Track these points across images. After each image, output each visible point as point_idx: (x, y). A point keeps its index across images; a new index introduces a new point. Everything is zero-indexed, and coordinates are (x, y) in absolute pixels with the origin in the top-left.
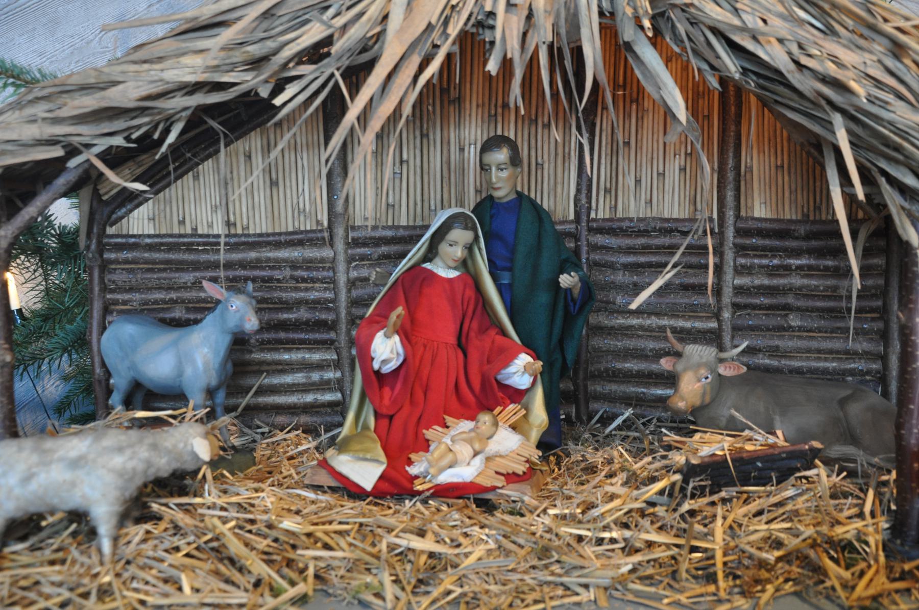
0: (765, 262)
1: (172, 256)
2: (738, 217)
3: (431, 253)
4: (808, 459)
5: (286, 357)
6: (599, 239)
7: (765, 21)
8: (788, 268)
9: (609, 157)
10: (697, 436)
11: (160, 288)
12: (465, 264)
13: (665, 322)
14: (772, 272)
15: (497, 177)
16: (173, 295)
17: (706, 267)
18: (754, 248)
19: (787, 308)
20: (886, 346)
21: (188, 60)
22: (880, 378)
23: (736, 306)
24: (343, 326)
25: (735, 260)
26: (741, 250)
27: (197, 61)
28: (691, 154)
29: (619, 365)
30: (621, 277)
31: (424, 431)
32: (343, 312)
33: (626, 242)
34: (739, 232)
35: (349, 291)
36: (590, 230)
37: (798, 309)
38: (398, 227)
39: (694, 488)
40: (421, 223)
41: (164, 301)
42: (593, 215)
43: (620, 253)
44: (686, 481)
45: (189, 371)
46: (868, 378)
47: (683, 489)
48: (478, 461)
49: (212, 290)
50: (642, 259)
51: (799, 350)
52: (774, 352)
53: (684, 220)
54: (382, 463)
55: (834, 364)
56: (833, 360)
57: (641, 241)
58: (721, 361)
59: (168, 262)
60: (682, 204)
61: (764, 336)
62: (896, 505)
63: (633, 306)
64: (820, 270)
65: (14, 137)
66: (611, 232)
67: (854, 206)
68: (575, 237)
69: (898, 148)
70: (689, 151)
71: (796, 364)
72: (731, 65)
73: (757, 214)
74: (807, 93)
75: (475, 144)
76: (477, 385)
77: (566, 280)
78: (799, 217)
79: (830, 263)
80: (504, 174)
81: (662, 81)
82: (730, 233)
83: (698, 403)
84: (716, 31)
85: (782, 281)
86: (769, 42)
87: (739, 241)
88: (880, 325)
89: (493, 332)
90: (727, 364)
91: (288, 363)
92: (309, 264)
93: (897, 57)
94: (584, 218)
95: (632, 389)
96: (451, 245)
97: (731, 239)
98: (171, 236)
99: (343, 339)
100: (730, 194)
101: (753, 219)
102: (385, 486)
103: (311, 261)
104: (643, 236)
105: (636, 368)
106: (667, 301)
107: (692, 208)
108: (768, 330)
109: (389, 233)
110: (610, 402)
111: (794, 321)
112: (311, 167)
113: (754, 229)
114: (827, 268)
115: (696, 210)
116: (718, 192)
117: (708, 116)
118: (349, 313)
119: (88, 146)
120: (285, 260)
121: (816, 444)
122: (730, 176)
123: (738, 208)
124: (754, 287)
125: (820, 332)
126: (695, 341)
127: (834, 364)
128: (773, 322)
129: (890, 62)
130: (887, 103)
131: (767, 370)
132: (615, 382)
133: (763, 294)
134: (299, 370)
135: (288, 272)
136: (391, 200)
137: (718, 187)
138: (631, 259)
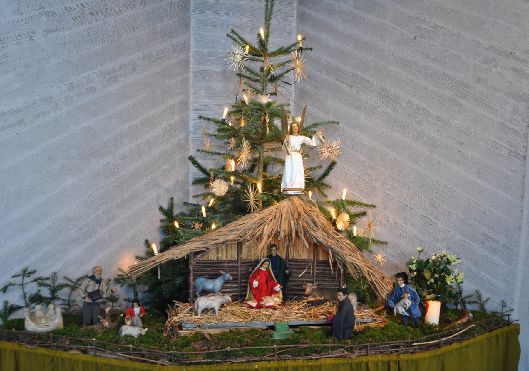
0: (322, 268)
1: (206, 265)
2: (317, 259)
3: (261, 266)
5: (228, 285)
6: (290, 263)
8: (326, 269)
10: (309, 298)
11: (203, 271)
12: (267, 269)
13: (303, 279)
14: (323, 270)
16: (206, 273)
17: (311, 269)
18: (320, 265)
19: (325, 277)
21: (231, 236)
23: (316, 276)
24: (239, 279)
26: (317, 266)
27: (232, 236)
29: (294, 288)
30: (295, 270)
32: (240, 277)
34: (317, 262)
35: (241, 272)
36: (289, 261)
37: (327, 277)
41: (204, 274)
42: (289, 258)
44: (307, 304)
45: (216, 288)
47: (307, 306)
49: (221, 272)
50: (299, 267)
51: (327, 285)
52: (323, 285)
58: (313, 286)
59: (205, 266)
63: (299, 276)
65: (198, 247)
68: (286, 262)
69: (338, 254)
71: (327, 287)
76: (270, 290)
77: (287, 272)
80: (275, 252)
82: (315, 263)
83: (309, 293)
84: (313, 236)
85: (325, 272)
87: (317, 264)
89: (272, 281)
91: (228, 287)
92: (233, 267)
94: (287, 258)
95: (296, 293)
98: (206, 261)
99: (239, 282)
100: (316, 255)
102: (257, 307)
103: (234, 266)
109: (249, 261)
111: (327, 279)
112: (234, 247)
118: (241, 277)
119: (210, 248)
120: (229, 266)
121: (328, 299)
123: (317, 258)
126: (309, 283)
128: (323, 279)
129: (337, 242)
131: (322, 288)
134: (230, 288)
135: (229, 268)
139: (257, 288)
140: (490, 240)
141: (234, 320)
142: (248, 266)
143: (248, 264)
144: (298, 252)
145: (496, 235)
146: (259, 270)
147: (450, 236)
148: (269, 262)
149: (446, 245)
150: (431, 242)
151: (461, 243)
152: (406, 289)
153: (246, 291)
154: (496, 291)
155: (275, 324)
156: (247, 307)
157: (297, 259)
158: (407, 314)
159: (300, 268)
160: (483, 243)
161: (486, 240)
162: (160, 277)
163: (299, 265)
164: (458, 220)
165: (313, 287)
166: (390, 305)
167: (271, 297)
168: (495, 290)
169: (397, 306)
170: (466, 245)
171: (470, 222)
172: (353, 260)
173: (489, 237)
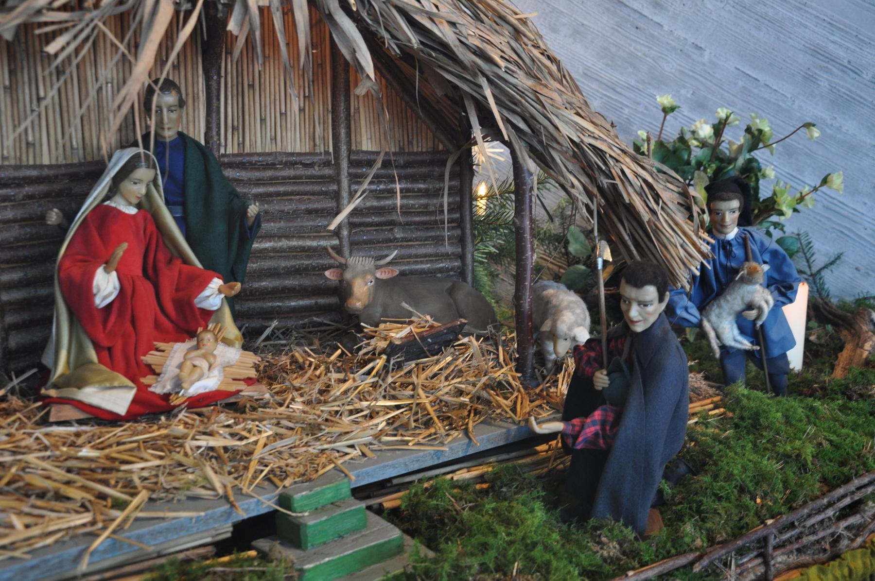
2: (350, 150)
3: (114, 190)
4: (457, 332)
7: (437, 7)
9: (235, 98)
12: (145, 205)
15: (168, 118)
20: (464, 248)
22: (460, 273)
25: (350, 187)
28: (309, 97)
29: (256, 285)
31: (142, 358)
33: (257, 174)
34: (352, 163)
38: (42, 167)
39: (394, 365)
40: (64, 162)
42: (222, 151)
43: (250, 184)
46: (451, 273)
48: (216, 372)
50: (271, 189)
53: (305, 154)
54: (132, 388)
55: (428, 266)
56: (427, 262)
57: (269, 173)
60: (303, 140)
61: (375, 248)
62: (518, 353)
64: (414, 192)
66: (241, 166)
67: (436, 140)
70: (307, 94)
72: (414, 40)
73: (364, 148)
74: (466, 63)
75: (112, 83)
78: (397, 150)
79: (422, 186)
80: (174, 116)
81: (358, 46)
82: (344, 164)
86: (441, 23)
87: (352, 171)
88: (458, 232)
89: (178, 263)
90: (383, 270)
93: (517, 40)
96: (135, 183)
97: (346, 169)
100: (343, 132)
101: (363, 152)
104: (271, 169)
105: (271, 285)
106: (296, 224)
107: (312, 143)
108: (379, 242)
109: (34, 173)
110: (248, 318)
111: (399, 234)
113: (364, 160)
114: (420, 190)
115: (315, 145)
116: (333, 129)
117: (321, 64)
122: (342, 115)
123: (349, 143)
124: (366, 208)
125: (417, 240)
127: (428, 266)
128: (381, 236)
129: (513, 43)
130: (513, 72)
132: (252, 300)
133: (373, 214)
136: (30, 139)
137: (333, 125)
138: (261, 190)
139: (109, 306)
140: (834, 70)
141: (35, 531)
142: (30, 197)
143: (28, 189)
144: (263, 121)
145: (853, 51)
146: (103, 213)
147: (704, 64)
148: (155, 167)
149: (689, 96)
150: (641, 86)
151: (740, 83)
152: (750, 244)
153: (47, 322)
154: (849, 229)
155: (285, 501)
156: (80, 422)
157: (259, 155)
158: (746, 344)
159: (278, 194)
160: (809, 79)
161: (821, 68)
162: (404, 308)
163: (272, 179)
164: (728, 8)
165: (381, 275)
166: (685, 315)
167: (191, 343)
168: (845, 227)
169: (713, 318)
170: (756, 91)
171: (771, 13)
172: (583, 130)
173: (832, 59)
